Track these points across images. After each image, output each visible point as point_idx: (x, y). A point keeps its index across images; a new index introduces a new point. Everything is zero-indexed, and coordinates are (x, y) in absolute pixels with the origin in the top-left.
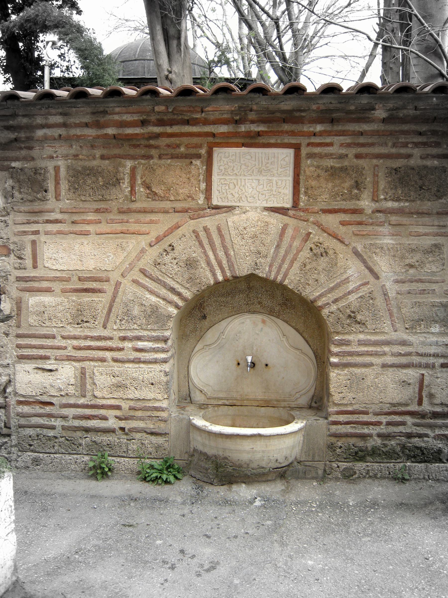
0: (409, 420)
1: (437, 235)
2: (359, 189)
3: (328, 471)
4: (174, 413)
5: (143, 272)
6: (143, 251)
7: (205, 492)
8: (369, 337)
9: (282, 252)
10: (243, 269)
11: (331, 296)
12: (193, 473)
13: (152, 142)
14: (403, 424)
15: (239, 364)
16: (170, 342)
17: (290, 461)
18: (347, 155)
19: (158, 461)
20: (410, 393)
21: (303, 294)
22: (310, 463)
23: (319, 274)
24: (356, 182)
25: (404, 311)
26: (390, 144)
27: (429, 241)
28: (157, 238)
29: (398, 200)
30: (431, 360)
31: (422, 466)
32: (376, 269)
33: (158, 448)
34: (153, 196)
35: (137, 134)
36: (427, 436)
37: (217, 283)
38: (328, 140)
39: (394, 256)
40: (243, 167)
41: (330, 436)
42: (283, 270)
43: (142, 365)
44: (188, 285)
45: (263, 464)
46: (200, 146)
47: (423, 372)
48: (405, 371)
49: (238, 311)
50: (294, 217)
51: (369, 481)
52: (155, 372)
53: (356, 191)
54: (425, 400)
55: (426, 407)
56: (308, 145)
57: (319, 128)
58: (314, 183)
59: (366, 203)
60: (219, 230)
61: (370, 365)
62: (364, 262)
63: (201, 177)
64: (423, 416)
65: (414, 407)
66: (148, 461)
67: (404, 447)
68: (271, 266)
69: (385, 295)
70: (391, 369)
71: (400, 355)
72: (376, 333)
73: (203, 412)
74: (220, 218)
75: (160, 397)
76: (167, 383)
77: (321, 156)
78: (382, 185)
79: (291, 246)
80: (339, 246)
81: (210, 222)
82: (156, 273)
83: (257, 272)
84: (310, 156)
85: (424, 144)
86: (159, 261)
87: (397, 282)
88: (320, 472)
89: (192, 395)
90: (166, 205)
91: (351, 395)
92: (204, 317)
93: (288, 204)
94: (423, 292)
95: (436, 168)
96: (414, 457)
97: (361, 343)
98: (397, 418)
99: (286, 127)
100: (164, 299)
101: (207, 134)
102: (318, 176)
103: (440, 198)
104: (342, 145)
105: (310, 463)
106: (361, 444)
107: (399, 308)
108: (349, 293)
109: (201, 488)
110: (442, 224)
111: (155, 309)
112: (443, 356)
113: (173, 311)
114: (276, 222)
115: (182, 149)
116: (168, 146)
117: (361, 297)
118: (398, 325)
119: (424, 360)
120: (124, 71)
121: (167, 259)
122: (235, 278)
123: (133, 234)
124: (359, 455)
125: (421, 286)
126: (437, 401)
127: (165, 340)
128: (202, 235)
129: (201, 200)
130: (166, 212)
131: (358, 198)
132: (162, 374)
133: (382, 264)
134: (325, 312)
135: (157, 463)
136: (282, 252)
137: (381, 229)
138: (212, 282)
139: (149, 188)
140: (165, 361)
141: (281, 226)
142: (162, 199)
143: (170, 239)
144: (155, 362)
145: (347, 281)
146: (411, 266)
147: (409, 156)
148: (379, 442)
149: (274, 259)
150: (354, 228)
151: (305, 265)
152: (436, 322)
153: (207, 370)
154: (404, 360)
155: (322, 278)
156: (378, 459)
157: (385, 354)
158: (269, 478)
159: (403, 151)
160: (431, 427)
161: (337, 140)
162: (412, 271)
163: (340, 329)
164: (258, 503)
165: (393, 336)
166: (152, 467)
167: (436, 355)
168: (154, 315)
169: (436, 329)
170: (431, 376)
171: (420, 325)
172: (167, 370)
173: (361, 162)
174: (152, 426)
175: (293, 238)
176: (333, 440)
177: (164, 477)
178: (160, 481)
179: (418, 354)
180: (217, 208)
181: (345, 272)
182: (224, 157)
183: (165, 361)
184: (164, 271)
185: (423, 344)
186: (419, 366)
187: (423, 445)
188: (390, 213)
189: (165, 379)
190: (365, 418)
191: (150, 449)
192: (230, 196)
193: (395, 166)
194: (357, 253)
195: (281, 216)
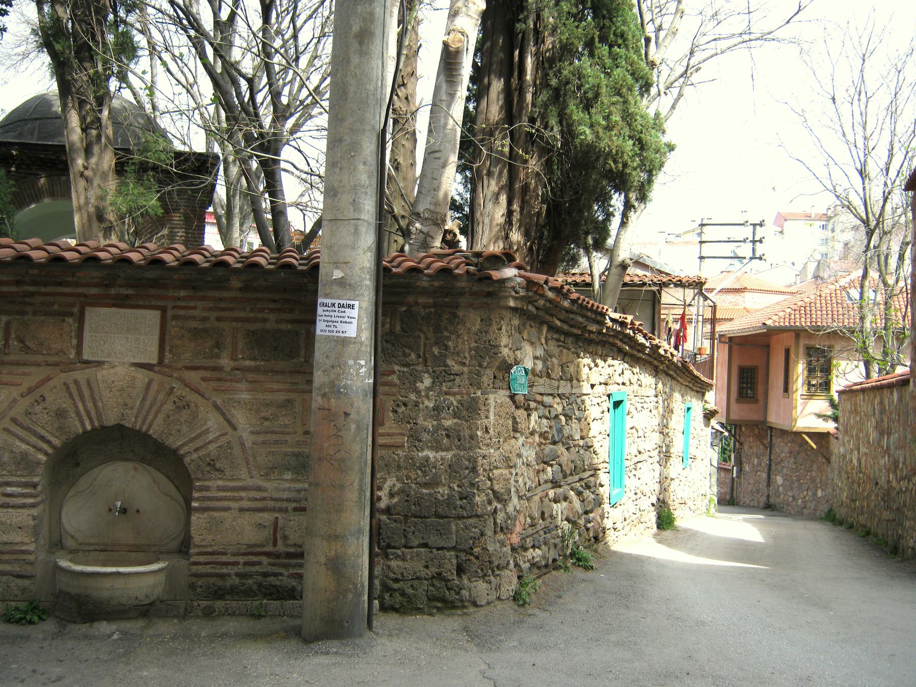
0: (265, 560)
1: (290, 391)
2: (219, 349)
3: (189, 610)
4: (42, 556)
5: (14, 420)
6: (15, 401)
7: (67, 629)
8: (227, 483)
9: (148, 404)
10: (111, 419)
11: (193, 446)
12: (57, 613)
13: (27, 300)
14: (260, 563)
15: (110, 510)
16: (39, 488)
17: (152, 599)
18: (209, 318)
19: (24, 604)
20: (266, 534)
21: (167, 443)
22: (172, 602)
23: (181, 425)
24: (217, 342)
25: (259, 459)
26: (248, 309)
27: (281, 397)
28: (29, 389)
29: (255, 359)
30: (285, 504)
31: (278, 603)
32: (234, 421)
33: (24, 590)
34: (27, 349)
35: (12, 292)
36: (282, 574)
37: (85, 432)
38: (192, 304)
39: (250, 410)
40: (113, 325)
41: (192, 575)
42: (148, 421)
43: (10, 510)
44: (57, 434)
45: (123, 601)
46: (73, 305)
47: (277, 515)
48: (260, 515)
49: (110, 459)
50: (160, 373)
51: (228, 618)
52: (24, 517)
53: (216, 350)
54: (280, 542)
55: (281, 547)
56: (174, 307)
57: (183, 293)
58: (178, 342)
59: (225, 362)
60: (89, 383)
61: (229, 509)
62: (223, 414)
63: (73, 334)
64: (278, 556)
65: (269, 548)
66: (13, 604)
67: (260, 585)
68: (136, 417)
69: (242, 444)
70: (247, 513)
71: (256, 499)
72: (233, 480)
73: (71, 556)
74: (89, 372)
75: (27, 540)
76: (35, 527)
77: (185, 318)
78: (240, 345)
79: (155, 399)
80: (200, 400)
81: (80, 375)
82: (26, 422)
83: (123, 422)
84: (175, 318)
85: (279, 310)
86: (30, 410)
87: (252, 433)
88: (182, 611)
89: (64, 541)
90: (40, 358)
91: (210, 537)
92: (78, 464)
93: (155, 362)
94: (276, 442)
95: (289, 332)
96: (270, 594)
97: (220, 489)
98: (254, 559)
99: (153, 292)
100: (34, 447)
101: (79, 295)
102: (183, 336)
103: (293, 358)
104: (204, 309)
105: (172, 602)
106: (220, 583)
107: (255, 457)
108: (209, 443)
109: (64, 627)
110: (294, 381)
111: (24, 456)
112: (295, 501)
113: (42, 457)
114: (142, 376)
115: (56, 307)
116: (43, 304)
117: (219, 447)
118: (254, 473)
119: (278, 505)
120: (40, 132)
121: (38, 409)
122: (103, 428)
123: (6, 384)
124: (219, 594)
125: (275, 437)
126: (290, 542)
127: (35, 486)
128: (73, 387)
129: (72, 355)
130: (38, 365)
131: (218, 357)
132: (30, 518)
133: (239, 416)
134: (187, 460)
135: (23, 606)
136: (148, 404)
137: (238, 385)
138: (81, 431)
139: (22, 341)
140: (33, 506)
141: (146, 380)
142: (35, 353)
143: (44, 390)
144: (24, 506)
145: (207, 431)
146: (266, 419)
147: (265, 320)
148: (237, 580)
149: (139, 411)
150: (214, 384)
151: (168, 417)
152: (288, 469)
153: (78, 517)
154: (259, 504)
155: (185, 428)
156: (236, 597)
157: (241, 499)
158: (131, 616)
159: (260, 315)
160: (285, 566)
161: (200, 304)
162: (266, 423)
163: (200, 475)
164: (115, 637)
165: (250, 482)
166: (17, 609)
167: (288, 500)
168: (24, 462)
169: (288, 476)
170: (285, 519)
171: (274, 473)
172: (35, 514)
173: (221, 325)
174: (18, 569)
175: (158, 392)
176: (194, 579)
177: (28, 617)
178: (24, 621)
179: (272, 499)
180: (87, 362)
181: (205, 424)
182: (96, 316)
183: (33, 506)
184: (34, 419)
185: (277, 489)
186: (274, 510)
187: (278, 583)
188: (247, 371)
189: (32, 523)
190: (224, 559)
191: (16, 592)
192: (100, 352)
193: (252, 329)
194: (217, 407)
195: (146, 371)
